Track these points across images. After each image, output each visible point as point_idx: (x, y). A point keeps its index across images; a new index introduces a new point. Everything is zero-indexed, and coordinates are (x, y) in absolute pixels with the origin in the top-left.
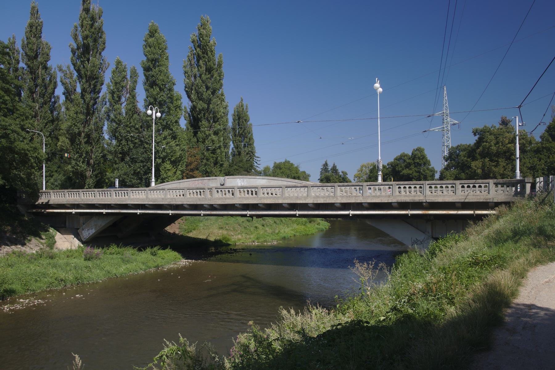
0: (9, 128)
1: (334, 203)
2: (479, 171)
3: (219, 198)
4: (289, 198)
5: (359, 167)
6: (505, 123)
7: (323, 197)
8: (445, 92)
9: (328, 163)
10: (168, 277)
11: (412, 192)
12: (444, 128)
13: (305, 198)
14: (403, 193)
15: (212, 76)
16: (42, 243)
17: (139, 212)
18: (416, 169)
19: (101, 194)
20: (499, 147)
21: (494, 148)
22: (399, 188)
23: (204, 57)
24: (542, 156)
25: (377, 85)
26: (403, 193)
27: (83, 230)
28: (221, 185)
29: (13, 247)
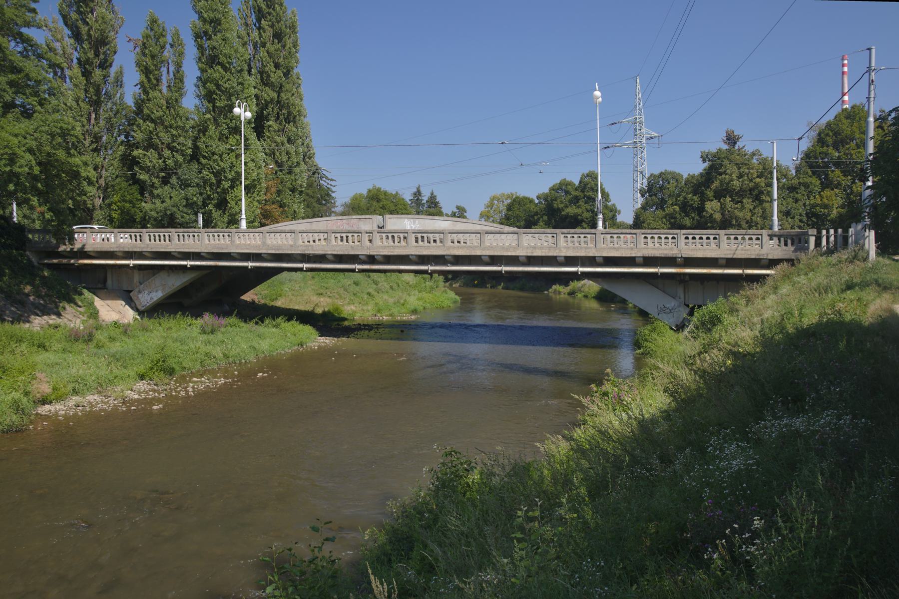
0: (72, 132)
1: (556, 257)
2: (718, 216)
3: (382, 247)
4: (491, 247)
5: (486, 200)
6: (731, 139)
7: (541, 248)
8: (639, 87)
9: (422, 190)
10: (300, 361)
11: (582, 244)
12: (636, 143)
13: (515, 249)
14: (650, 245)
15: (284, 46)
16: (81, 313)
17: (250, 264)
18: (589, 207)
19: (211, 237)
20: (743, 181)
21: (736, 184)
22: (646, 238)
23: (269, 14)
24: (799, 196)
25: (597, 93)
26: (650, 245)
27: (140, 292)
28: (379, 227)
29: (45, 317)
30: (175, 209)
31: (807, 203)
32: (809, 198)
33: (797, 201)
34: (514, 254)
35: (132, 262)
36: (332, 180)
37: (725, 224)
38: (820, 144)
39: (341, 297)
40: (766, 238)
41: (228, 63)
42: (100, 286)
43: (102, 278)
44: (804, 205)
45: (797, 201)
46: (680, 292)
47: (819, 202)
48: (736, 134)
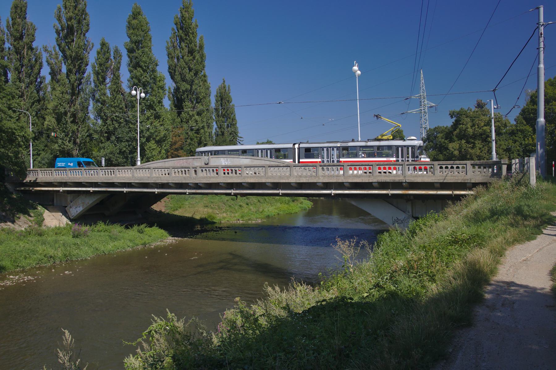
2: (456, 153)
3: (204, 177)
4: (272, 177)
7: (306, 177)
8: (422, 76)
12: (421, 110)
13: (288, 177)
15: (194, 58)
16: (30, 221)
17: (125, 190)
20: (475, 129)
21: (470, 131)
23: (186, 39)
24: (517, 138)
25: (356, 68)
27: (71, 207)
30: (111, 155)
31: (523, 143)
32: (524, 140)
33: (515, 141)
34: (287, 181)
35: (61, 189)
36: (241, 137)
37: (463, 157)
38: (532, 104)
39: (219, 208)
40: (469, 167)
41: (145, 66)
42: (51, 203)
43: (51, 200)
44: (521, 144)
45: (515, 141)
46: (409, 208)
47: (531, 142)
48: (483, 102)
